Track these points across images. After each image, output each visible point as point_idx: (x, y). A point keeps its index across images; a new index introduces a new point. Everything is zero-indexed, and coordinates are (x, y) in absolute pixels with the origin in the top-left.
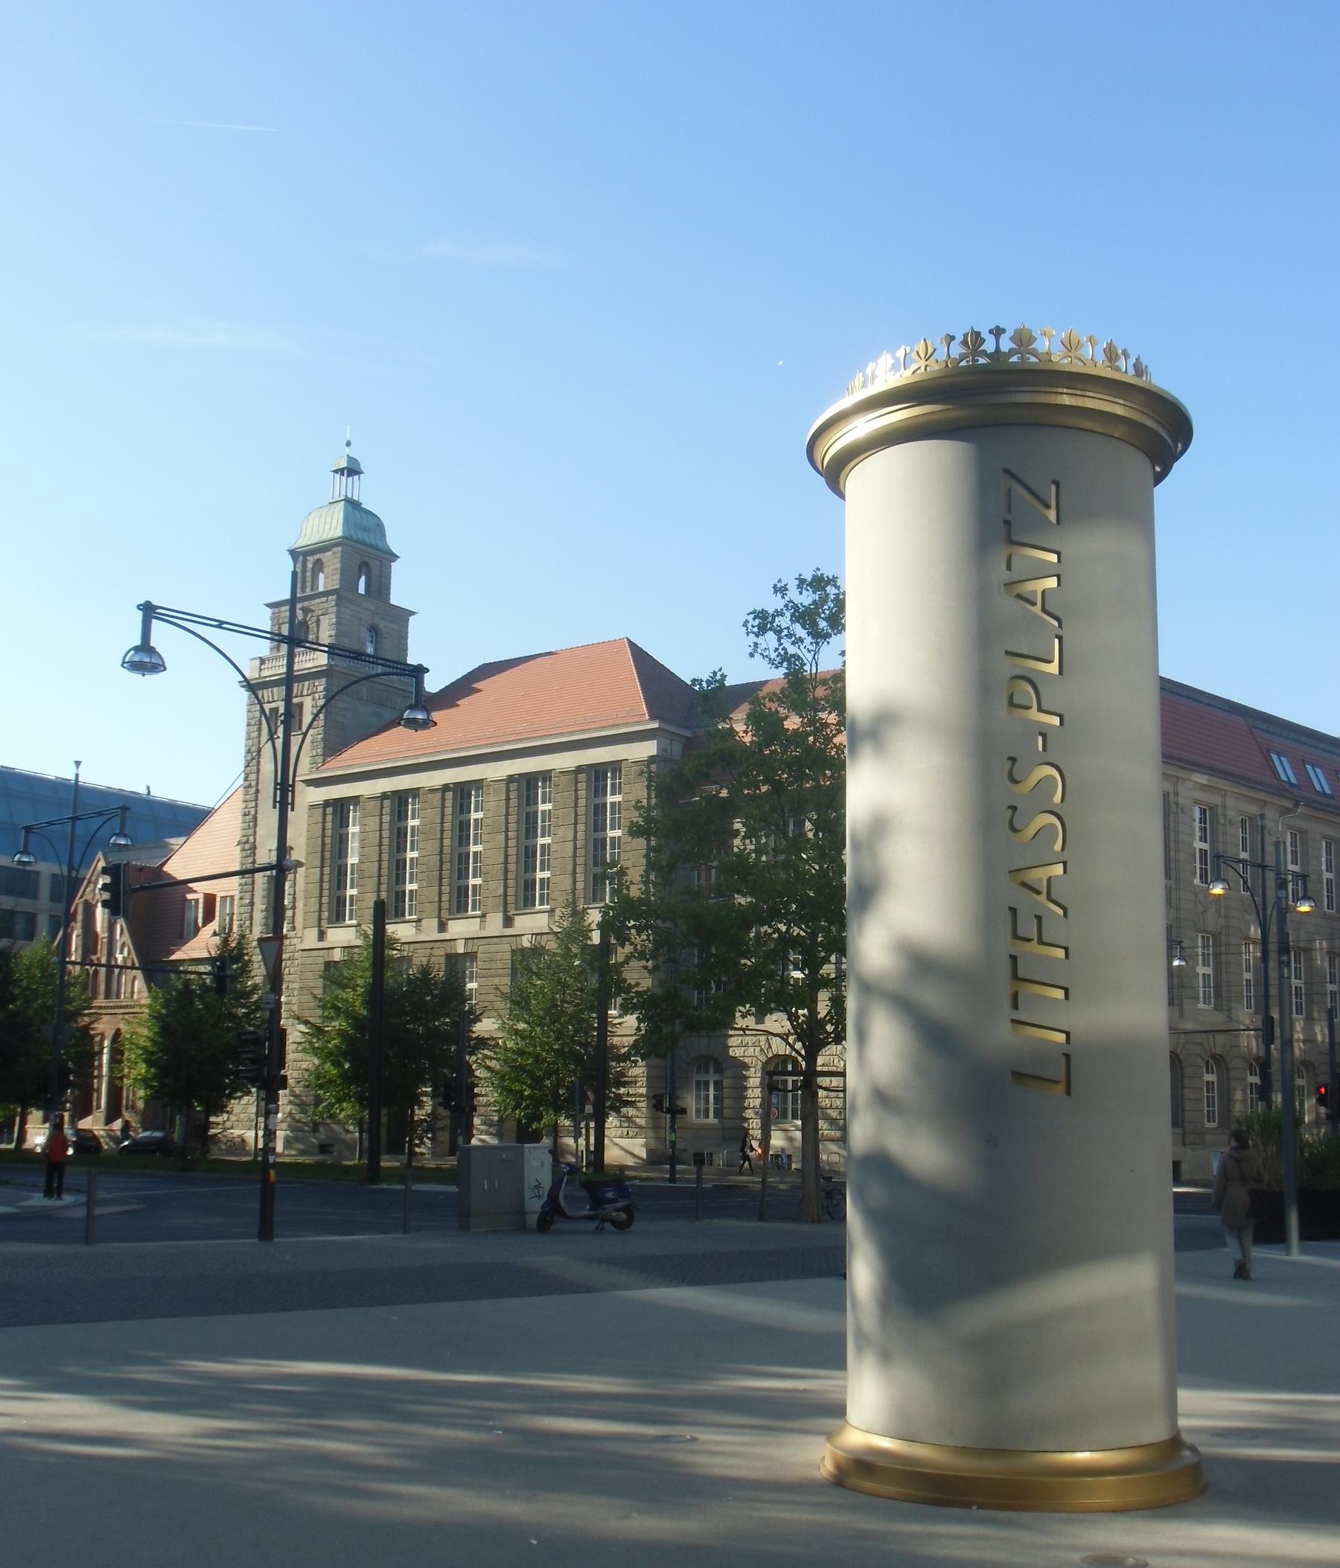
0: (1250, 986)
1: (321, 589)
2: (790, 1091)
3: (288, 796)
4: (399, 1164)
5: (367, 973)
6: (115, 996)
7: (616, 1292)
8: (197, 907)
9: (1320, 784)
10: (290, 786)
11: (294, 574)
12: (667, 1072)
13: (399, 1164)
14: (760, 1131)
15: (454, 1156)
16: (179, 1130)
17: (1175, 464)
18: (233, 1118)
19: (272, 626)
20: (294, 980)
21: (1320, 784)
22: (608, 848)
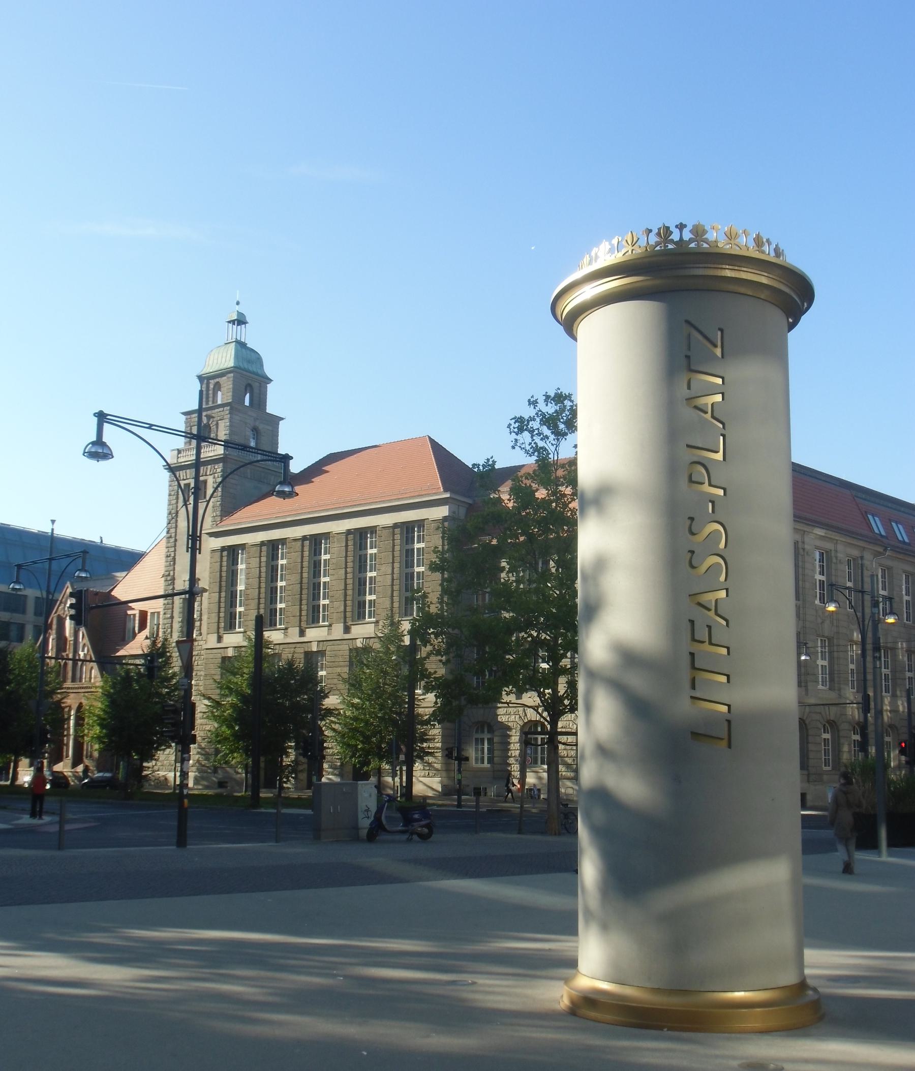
0: (854, 673)
1: (219, 402)
2: (540, 745)
3: (196, 544)
4: (272, 795)
5: (251, 665)
6: (78, 680)
7: (421, 883)
8: (134, 620)
9: (902, 535)
10: (198, 537)
11: (201, 392)
12: (455, 732)
13: (272, 795)
14: (519, 773)
15: (310, 789)
16: (122, 772)
17: (802, 317)
18: (159, 764)
19: (186, 427)
20: (201, 670)
21: (902, 535)
22: (415, 579)
